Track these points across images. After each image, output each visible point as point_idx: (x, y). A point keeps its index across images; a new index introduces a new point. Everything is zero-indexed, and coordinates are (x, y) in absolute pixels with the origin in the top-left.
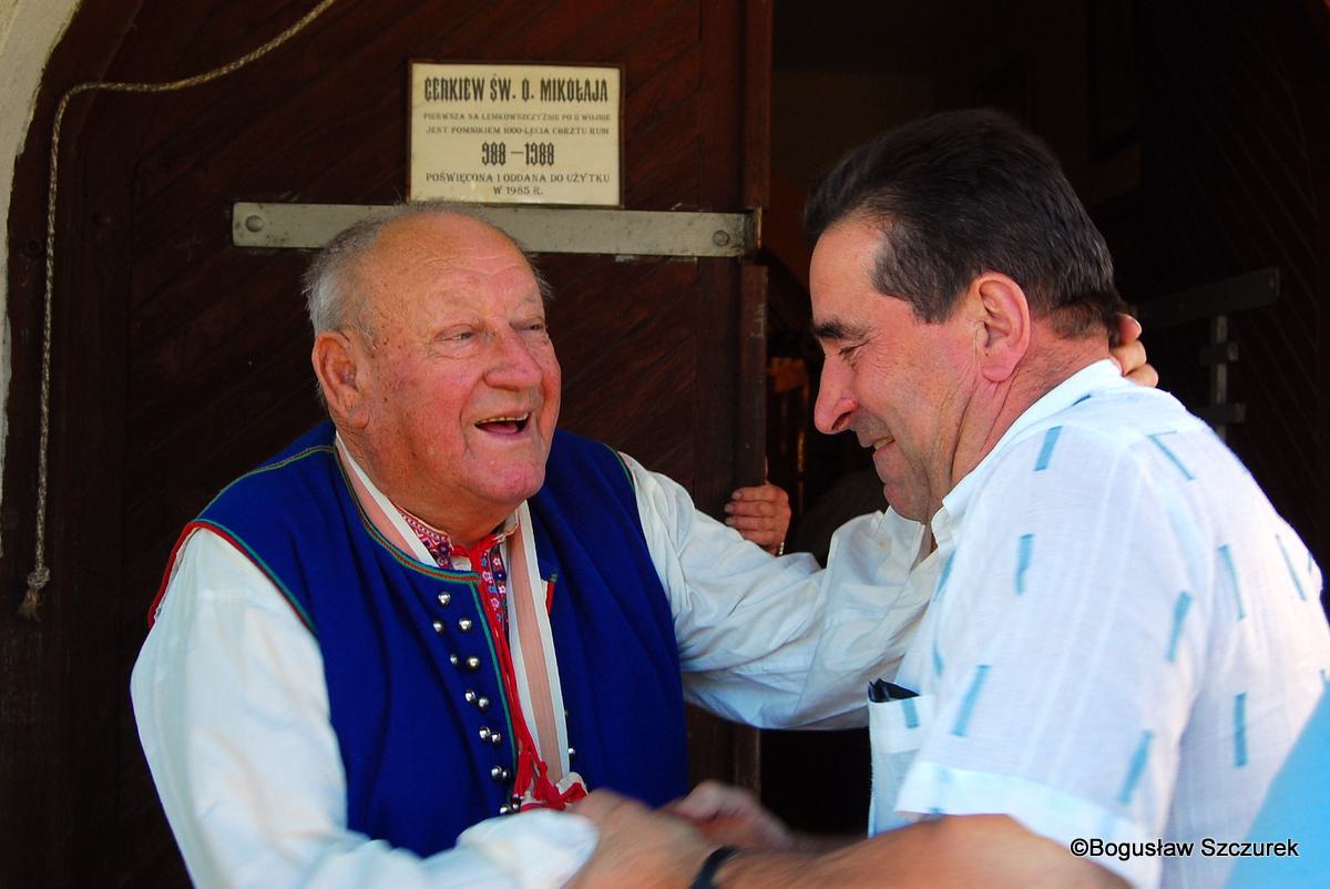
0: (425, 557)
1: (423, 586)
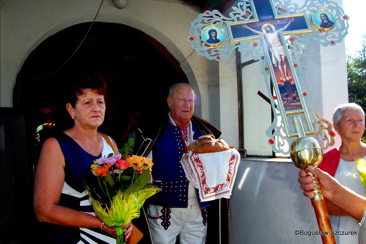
0: (175, 125)
1: (174, 127)
